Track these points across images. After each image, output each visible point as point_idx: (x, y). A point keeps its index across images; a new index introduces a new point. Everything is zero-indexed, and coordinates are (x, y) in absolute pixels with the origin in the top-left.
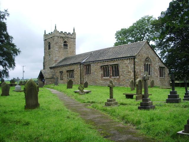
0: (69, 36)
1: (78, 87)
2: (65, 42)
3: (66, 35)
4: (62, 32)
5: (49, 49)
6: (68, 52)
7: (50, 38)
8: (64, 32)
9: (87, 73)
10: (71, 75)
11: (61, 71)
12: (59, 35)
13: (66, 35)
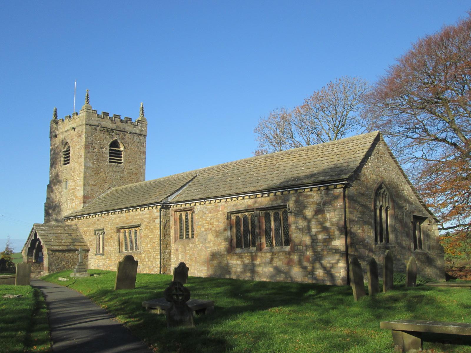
0: (128, 127)
1: (215, 249)
2: (115, 144)
3: (119, 124)
4: (106, 114)
5: (65, 164)
6: (122, 172)
7: (67, 131)
8: (111, 115)
9: (181, 237)
10: (131, 241)
11: (99, 228)
12: (96, 123)
13: (119, 124)
